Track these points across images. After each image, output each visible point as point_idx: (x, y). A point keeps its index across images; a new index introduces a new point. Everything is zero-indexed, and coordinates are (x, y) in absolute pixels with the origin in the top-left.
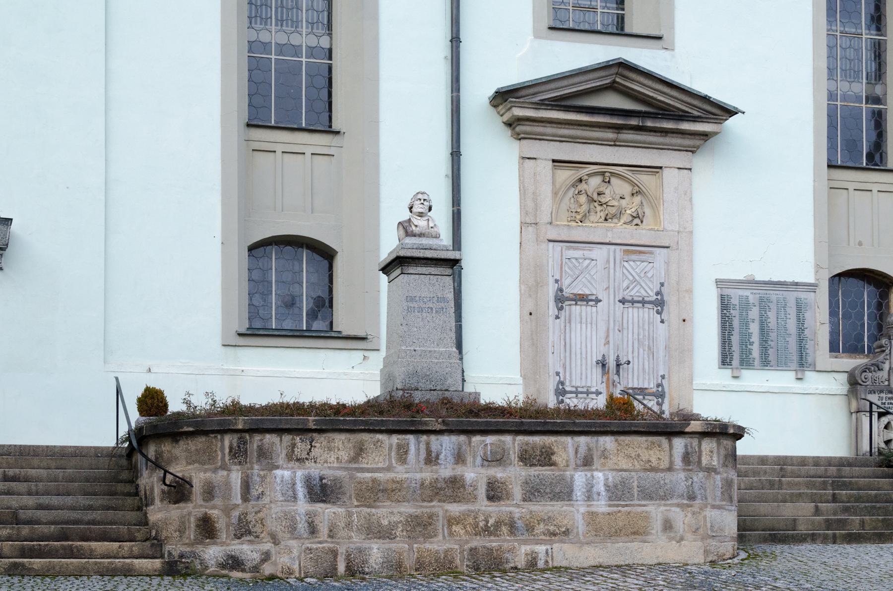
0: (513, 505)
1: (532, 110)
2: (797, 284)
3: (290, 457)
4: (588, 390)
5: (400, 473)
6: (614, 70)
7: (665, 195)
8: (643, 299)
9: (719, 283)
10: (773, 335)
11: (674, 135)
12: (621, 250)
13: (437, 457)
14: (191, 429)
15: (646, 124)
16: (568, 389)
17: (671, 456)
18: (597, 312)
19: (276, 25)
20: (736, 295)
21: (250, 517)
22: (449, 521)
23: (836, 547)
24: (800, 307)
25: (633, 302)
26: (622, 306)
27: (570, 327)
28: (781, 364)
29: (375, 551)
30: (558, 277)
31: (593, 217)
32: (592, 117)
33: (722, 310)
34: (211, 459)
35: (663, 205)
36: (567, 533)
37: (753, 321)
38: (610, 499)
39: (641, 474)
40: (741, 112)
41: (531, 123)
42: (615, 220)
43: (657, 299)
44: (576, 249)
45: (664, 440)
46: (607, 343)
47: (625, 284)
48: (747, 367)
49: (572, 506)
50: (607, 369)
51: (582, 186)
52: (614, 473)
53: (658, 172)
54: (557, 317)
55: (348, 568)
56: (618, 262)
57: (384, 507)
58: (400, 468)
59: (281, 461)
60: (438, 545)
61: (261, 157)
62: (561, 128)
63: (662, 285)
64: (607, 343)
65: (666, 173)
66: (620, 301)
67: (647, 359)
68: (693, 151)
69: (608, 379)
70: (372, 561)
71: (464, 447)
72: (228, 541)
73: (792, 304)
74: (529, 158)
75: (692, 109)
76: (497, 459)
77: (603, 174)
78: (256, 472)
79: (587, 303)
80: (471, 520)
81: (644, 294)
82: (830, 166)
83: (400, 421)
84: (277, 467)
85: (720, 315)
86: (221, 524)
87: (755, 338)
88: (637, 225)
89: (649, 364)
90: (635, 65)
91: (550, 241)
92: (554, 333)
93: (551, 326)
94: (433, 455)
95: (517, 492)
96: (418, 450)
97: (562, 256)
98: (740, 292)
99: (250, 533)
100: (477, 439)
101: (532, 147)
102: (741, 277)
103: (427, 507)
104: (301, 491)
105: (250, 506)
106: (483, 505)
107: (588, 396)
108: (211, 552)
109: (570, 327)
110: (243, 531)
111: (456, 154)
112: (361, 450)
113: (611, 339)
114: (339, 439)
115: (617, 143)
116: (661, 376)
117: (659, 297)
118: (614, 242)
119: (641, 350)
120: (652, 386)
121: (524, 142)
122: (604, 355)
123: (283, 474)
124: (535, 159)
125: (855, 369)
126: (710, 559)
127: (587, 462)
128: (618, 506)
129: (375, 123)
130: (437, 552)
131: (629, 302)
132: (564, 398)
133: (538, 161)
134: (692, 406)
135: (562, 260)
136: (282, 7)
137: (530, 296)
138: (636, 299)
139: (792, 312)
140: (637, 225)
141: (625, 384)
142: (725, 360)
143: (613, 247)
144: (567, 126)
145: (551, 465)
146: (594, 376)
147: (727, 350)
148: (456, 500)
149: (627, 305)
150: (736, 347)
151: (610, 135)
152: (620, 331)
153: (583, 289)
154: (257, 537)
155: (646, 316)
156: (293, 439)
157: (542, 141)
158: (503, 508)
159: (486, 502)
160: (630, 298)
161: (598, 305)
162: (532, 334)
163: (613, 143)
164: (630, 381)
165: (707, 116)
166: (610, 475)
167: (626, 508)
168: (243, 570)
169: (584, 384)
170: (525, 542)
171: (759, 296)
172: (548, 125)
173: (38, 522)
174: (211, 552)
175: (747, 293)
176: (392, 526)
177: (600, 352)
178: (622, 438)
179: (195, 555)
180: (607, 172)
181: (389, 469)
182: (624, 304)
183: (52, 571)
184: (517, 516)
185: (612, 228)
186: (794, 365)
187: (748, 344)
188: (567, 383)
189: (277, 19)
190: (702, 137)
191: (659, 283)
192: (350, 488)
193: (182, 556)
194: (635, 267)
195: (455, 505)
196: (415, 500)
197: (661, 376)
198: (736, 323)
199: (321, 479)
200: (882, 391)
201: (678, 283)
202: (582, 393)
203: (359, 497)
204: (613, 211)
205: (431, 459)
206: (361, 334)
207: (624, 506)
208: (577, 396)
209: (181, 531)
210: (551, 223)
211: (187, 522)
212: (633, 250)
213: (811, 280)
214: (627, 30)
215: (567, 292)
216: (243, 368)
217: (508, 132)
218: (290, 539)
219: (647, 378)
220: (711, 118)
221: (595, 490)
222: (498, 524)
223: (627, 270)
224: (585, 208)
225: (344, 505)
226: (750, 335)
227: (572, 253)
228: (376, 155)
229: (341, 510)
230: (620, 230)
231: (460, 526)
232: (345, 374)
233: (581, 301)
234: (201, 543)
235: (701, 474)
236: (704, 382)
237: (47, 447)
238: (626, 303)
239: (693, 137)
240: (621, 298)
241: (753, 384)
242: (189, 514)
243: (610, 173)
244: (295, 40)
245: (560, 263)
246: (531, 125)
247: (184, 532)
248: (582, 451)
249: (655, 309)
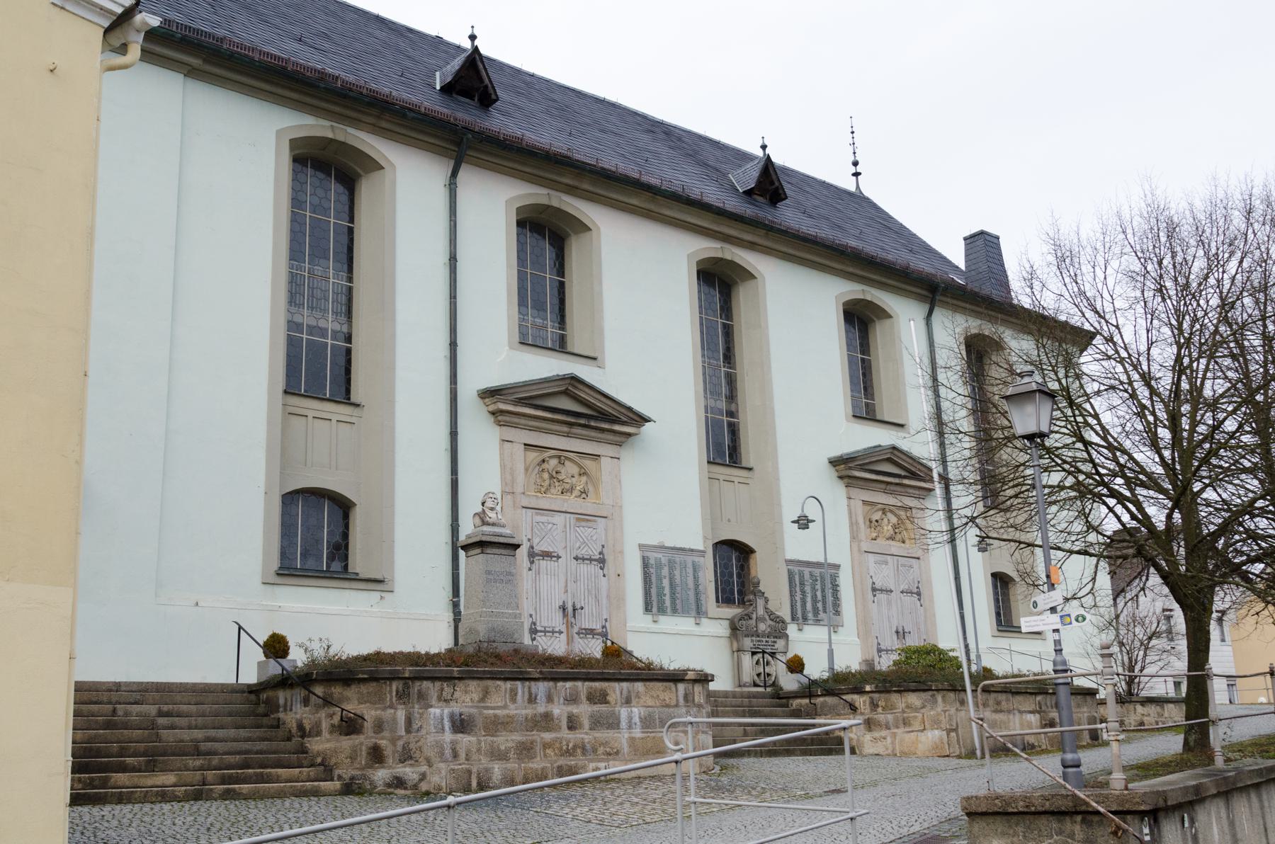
0: (583, 733)
2: (692, 550)
3: (440, 698)
5: (512, 710)
10: (678, 589)
13: (536, 698)
14: (366, 676)
16: (539, 628)
17: (677, 696)
19: (308, 309)
20: (653, 556)
21: (411, 746)
22: (544, 746)
23: (761, 759)
24: (696, 568)
25: (583, 559)
28: (685, 612)
29: (496, 770)
31: (553, 490)
34: (382, 700)
36: (617, 753)
38: (643, 728)
39: (660, 709)
42: (569, 494)
45: (672, 685)
46: (566, 591)
47: (578, 545)
49: (620, 733)
51: (545, 466)
52: (645, 709)
54: (530, 569)
55: (479, 784)
56: (572, 527)
57: (501, 736)
58: (512, 706)
59: (434, 702)
60: (536, 764)
61: (295, 420)
63: (603, 546)
64: (566, 591)
66: (574, 558)
68: (619, 445)
69: (567, 621)
70: (494, 778)
71: (552, 690)
72: (394, 765)
73: (690, 565)
76: (572, 699)
77: (559, 457)
78: (416, 710)
80: (558, 745)
81: (591, 553)
82: (709, 462)
83: (512, 672)
84: (431, 706)
86: (388, 751)
87: (667, 591)
92: (527, 581)
93: (525, 576)
94: (533, 696)
95: (586, 723)
96: (523, 692)
98: (656, 555)
99: (411, 758)
100: (560, 684)
101: (511, 433)
102: (655, 543)
103: (529, 736)
104: (447, 725)
105: (412, 737)
106: (565, 734)
108: (380, 774)
110: (406, 756)
111: (454, 434)
112: (487, 693)
114: (473, 685)
121: (504, 428)
123: (435, 711)
125: (734, 617)
126: (702, 770)
127: (628, 701)
128: (647, 732)
129: (391, 402)
130: (537, 770)
136: (313, 297)
138: (586, 557)
139: (690, 571)
142: (648, 608)
143: (568, 515)
145: (606, 703)
148: (548, 729)
149: (580, 561)
150: (654, 598)
151: (565, 429)
154: (417, 761)
156: (442, 685)
158: (578, 735)
159: (567, 731)
160: (581, 556)
166: (642, 710)
167: (652, 734)
168: (406, 788)
170: (592, 761)
173: (215, 753)
174: (380, 774)
175: (660, 556)
176: (508, 750)
178: (648, 683)
179: (365, 777)
180: (562, 456)
181: (505, 707)
183: (257, 795)
184: (586, 741)
186: (694, 613)
188: (538, 624)
189: (308, 307)
192: (479, 722)
193: (352, 778)
194: (585, 532)
195: (547, 733)
196: (522, 730)
198: (654, 578)
199: (461, 715)
200: (753, 636)
201: (614, 546)
203: (486, 728)
204: (567, 486)
205: (532, 699)
206: (379, 577)
207: (651, 733)
209: (353, 758)
210: (524, 493)
211: (359, 751)
212: (584, 518)
213: (702, 548)
214: (569, 349)
215: (537, 549)
216: (280, 604)
217: (492, 419)
218: (439, 762)
221: (633, 721)
222: (575, 747)
224: (547, 483)
225: (476, 735)
226: (663, 588)
227: (539, 518)
228: (393, 428)
229: (473, 739)
231: (551, 749)
232: (366, 612)
234: (371, 767)
235: (695, 709)
237: (181, 683)
242: (361, 744)
244: (322, 324)
247: (356, 759)
248: (625, 692)
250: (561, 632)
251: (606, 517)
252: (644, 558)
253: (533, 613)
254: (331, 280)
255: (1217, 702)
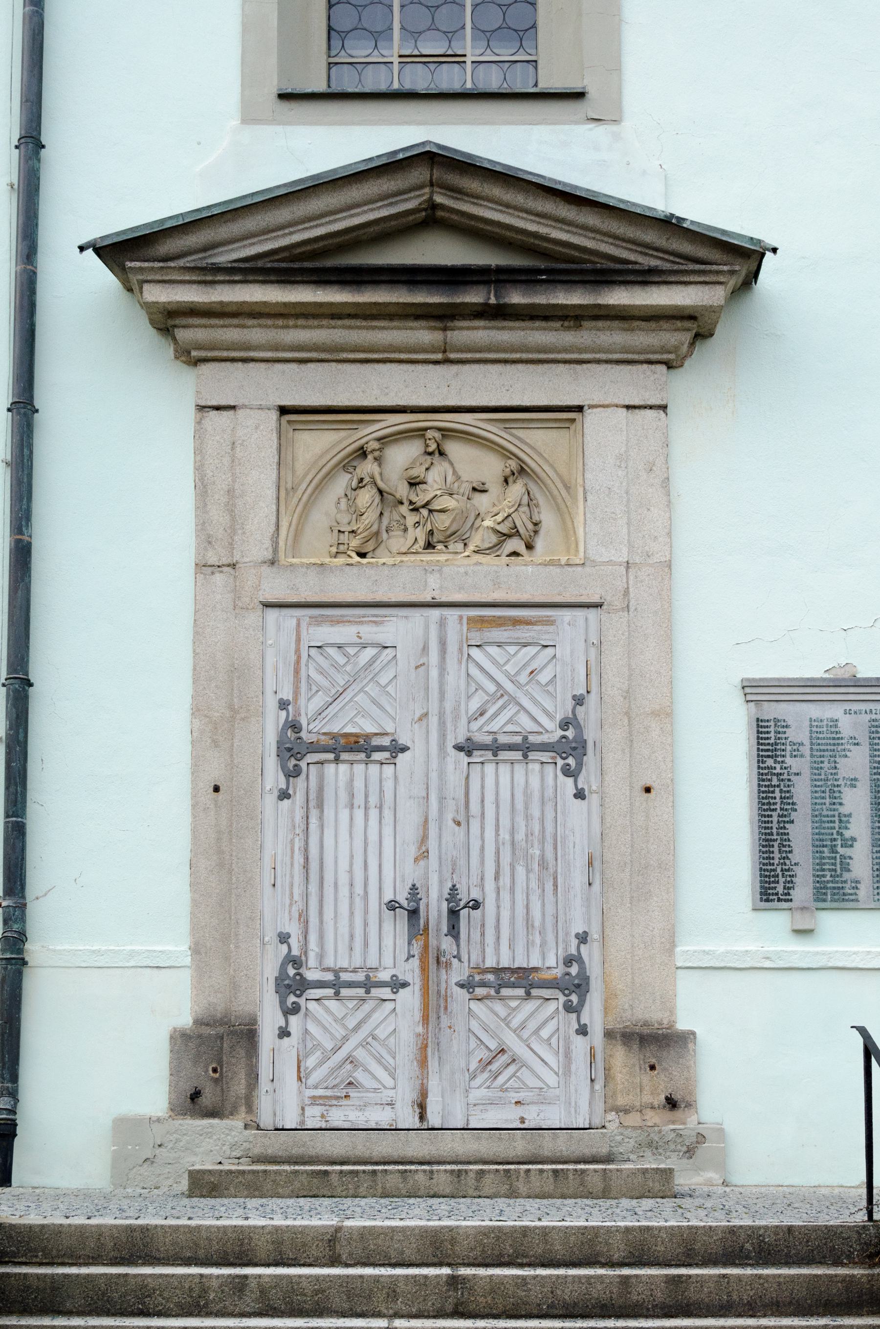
1: (195, 286)
4: (368, 977)
6: (419, 175)
7: (588, 475)
8: (525, 738)
9: (748, 690)
11: (600, 324)
12: (461, 617)
15: (507, 300)
16: (311, 975)
18: (396, 778)
25: (496, 748)
26: (467, 760)
27: (321, 818)
30: (287, 694)
31: (397, 542)
32: (359, 291)
33: (761, 759)
35: (585, 500)
37: (853, 783)
40: (769, 250)
41: (204, 321)
43: (564, 737)
44: (338, 622)
46: (424, 855)
47: (475, 704)
48: (835, 905)
50: (422, 922)
53: (573, 421)
54: (284, 795)
62: (287, 327)
63: (579, 701)
64: (424, 855)
65: (591, 418)
66: (459, 748)
67: (538, 892)
69: (426, 947)
74: (218, 408)
75: (646, 254)
79: (368, 756)
81: (529, 725)
85: (756, 771)
88: (515, 554)
89: (543, 905)
90: (470, 156)
91: (268, 605)
97: (298, 640)
102: (815, 671)
107: (368, 992)
109: (321, 818)
113: (432, 844)
115: (452, 356)
116: (577, 936)
117: (570, 733)
118: (444, 599)
119: (521, 871)
120: (551, 961)
122: (414, 887)
124: (233, 408)
131: (484, 747)
132: (302, 1001)
133: (240, 413)
134: (672, 1011)
135: (298, 651)
137: (216, 744)
138: (503, 739)
140: (515, 554)
141: (474, 958)
143: (436, 613)
144: (301, 322)
146: (388, 942)
147: (776, 861)
152: (459, 824)
153: (360, 721)
155: (535, 782)
157: (251, 365)
160: (488, 739)
161: (397, 761)
162: (219, 839)
163: (439, 356)
164: (490, 951)
165: (676, 267)
169: (357, 962)
171: (868, 717)
172: (250, 322)
177: (403, 881)
182: (469, 754)
185: (440, 565)
187: (839, 842)
188: (312, 961)
190: (679, 324)
191: (570, 697)
197: (577, 936)
198: (802, 791)
201: (628, 695)
202: (351, 985)
208: (337, 993)
210: (272, 563)
219: (538, 941)
220: (694, 272)
223: (482, 669)
226: (844, 820)
230: (462, 570)
233: (351, 750)
236: (707, 948)
238: (475, 753)
239: (653, 324)
240: (461, 739)
241: (855, 949)
243: (439, 429)
245: (293, 658)
246: (205, 327)
249: (560, 762)
250: (398, 985)
251: (598, 606)
252: (760, 727)
253: (294, 930)
254: (469, 59)
255: (676, 1182)
